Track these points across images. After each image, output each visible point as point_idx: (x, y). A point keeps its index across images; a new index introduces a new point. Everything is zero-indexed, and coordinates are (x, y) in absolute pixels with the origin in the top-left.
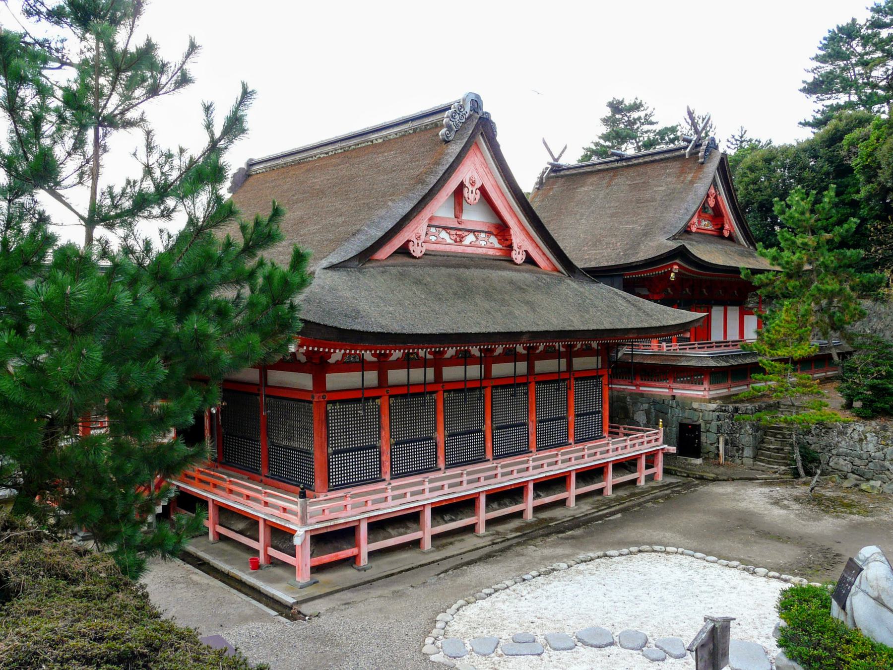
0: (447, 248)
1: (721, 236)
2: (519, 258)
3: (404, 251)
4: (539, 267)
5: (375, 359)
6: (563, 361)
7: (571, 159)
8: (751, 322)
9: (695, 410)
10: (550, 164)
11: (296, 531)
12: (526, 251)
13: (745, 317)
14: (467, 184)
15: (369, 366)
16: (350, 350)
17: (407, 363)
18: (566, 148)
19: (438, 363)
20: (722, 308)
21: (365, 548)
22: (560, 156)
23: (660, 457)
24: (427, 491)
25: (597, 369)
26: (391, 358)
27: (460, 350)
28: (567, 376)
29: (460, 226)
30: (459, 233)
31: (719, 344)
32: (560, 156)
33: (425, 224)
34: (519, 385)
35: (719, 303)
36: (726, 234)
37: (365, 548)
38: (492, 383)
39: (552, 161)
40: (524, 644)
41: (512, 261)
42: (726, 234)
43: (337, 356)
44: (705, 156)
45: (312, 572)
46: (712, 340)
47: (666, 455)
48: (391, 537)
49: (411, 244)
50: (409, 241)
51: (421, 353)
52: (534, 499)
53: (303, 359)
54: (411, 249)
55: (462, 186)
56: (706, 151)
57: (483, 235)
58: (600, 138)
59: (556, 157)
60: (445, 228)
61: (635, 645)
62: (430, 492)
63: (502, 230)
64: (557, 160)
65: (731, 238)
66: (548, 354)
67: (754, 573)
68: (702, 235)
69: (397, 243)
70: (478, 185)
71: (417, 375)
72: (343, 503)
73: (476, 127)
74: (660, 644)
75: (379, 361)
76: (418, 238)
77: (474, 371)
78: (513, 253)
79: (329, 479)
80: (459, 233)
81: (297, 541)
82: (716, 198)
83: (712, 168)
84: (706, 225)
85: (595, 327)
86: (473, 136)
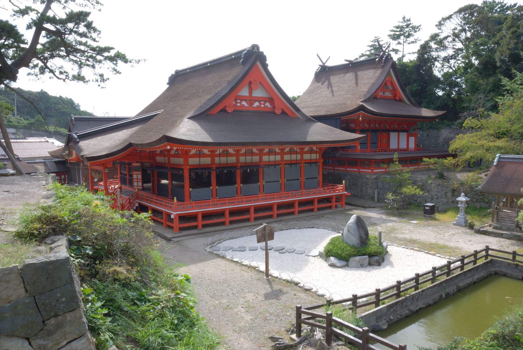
1: (396, 100)
3: (224, 110)
4: (287, 115)
5: (235, 153)
6: (166, 158)
8: (412, 140)
9: (367, 178)
12: (282, 109)
13: (410, 138)
17: (291, 152)
19: (302, 153)
22: (326, 61)
23: (344, 197)
32: (326, 61)
35: (394, 131)
38: (284, 162)
39: (322, 64)
43: (193, 152)
47: (346, 196)
51: (295, 149)
54: (227, 109)
60: (245, 100)
64: (324, 64)
65: (401, 100)
69: (221, 107)
71: (294, 157)
77: (278, 158)
81: (172, 217)
83: (390, 64)
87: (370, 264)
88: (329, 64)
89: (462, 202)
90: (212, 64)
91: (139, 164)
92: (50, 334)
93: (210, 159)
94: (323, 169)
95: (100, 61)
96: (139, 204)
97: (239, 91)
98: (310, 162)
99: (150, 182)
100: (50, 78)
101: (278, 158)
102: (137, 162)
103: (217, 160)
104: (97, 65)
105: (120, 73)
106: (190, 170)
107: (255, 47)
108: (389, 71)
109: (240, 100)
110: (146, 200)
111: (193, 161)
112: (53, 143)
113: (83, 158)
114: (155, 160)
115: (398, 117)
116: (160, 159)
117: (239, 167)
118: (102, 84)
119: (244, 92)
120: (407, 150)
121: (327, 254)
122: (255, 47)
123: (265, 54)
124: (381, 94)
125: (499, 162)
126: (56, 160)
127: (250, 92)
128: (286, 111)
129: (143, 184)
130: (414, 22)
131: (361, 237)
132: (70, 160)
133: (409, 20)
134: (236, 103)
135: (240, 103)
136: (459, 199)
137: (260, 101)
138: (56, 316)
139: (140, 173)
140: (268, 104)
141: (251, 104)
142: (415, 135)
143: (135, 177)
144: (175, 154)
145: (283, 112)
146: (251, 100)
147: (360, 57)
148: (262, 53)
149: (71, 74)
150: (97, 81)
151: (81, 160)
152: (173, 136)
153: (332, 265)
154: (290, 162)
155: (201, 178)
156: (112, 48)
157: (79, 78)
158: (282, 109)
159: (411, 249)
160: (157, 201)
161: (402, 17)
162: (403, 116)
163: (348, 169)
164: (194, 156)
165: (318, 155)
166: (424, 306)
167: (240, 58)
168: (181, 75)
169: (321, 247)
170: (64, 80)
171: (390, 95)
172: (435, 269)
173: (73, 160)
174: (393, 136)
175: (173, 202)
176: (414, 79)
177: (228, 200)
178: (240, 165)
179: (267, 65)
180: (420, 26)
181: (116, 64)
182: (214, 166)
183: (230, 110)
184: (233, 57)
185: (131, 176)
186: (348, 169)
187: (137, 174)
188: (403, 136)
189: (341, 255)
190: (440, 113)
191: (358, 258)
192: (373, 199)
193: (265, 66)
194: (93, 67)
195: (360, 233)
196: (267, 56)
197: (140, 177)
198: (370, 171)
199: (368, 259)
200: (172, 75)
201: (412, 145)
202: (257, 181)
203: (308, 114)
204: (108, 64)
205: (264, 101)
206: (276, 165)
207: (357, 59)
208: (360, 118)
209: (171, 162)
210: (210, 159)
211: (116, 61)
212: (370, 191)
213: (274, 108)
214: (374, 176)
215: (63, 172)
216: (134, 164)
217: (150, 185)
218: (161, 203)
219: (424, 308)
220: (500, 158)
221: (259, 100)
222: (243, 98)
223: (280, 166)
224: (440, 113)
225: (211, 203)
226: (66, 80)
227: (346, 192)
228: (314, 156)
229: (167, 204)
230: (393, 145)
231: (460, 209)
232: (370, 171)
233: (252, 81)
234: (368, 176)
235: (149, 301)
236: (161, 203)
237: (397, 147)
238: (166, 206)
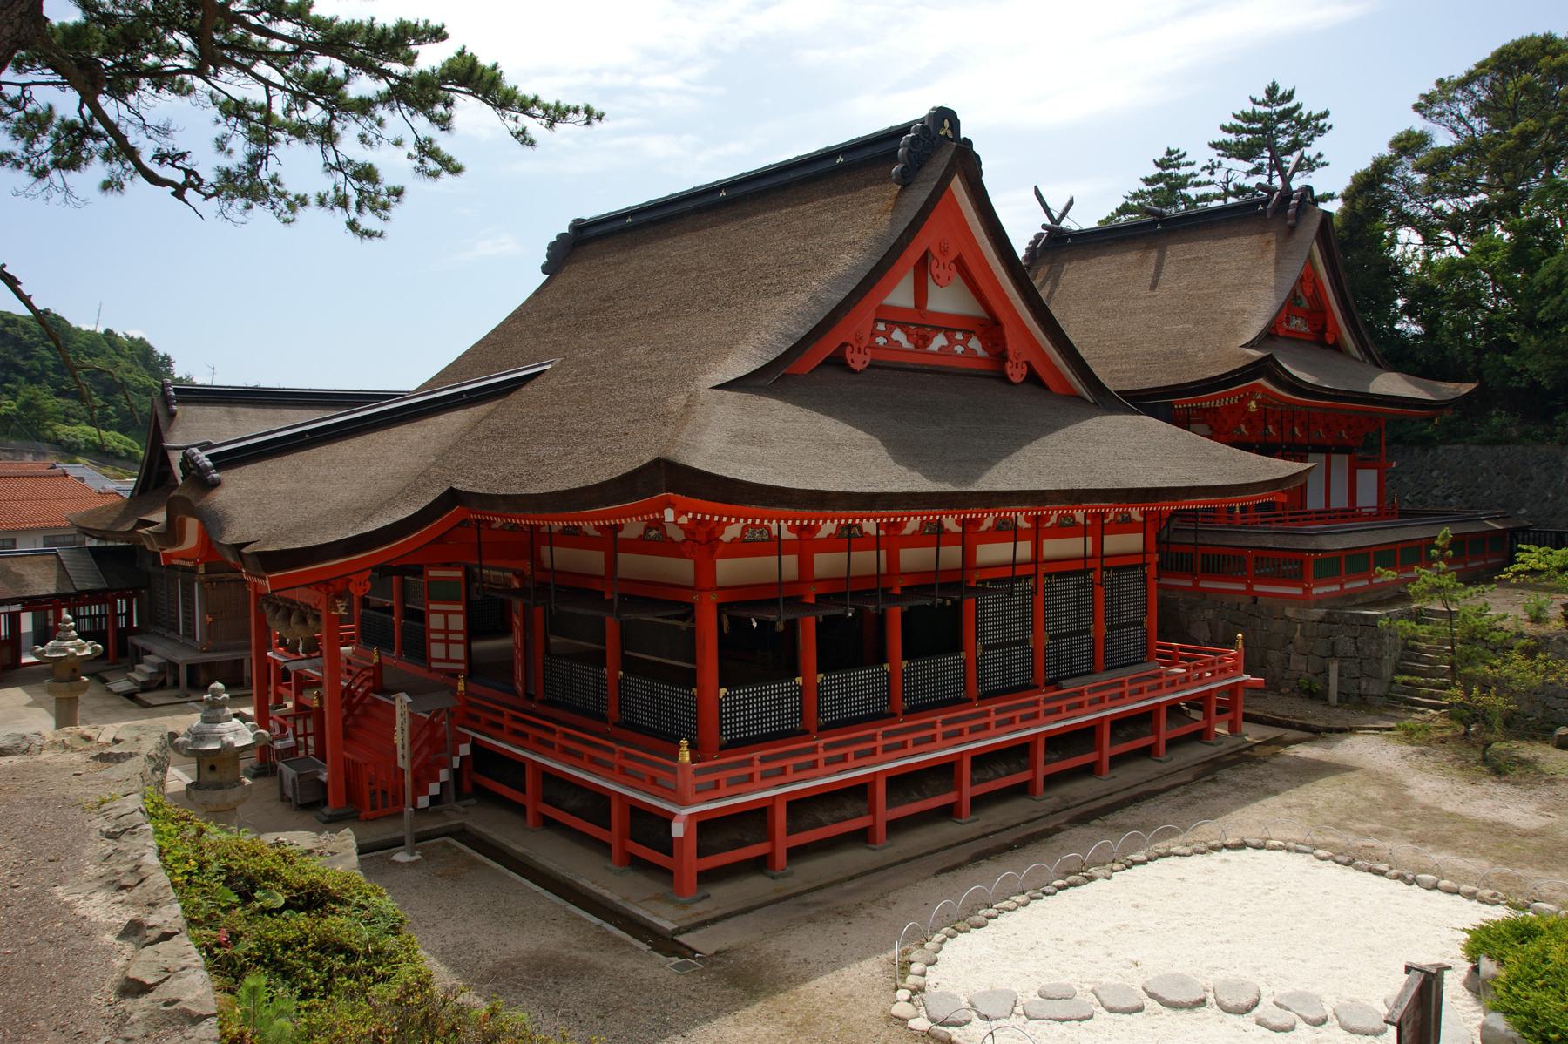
4: (1047, 388)
5: (794, 536)
7: (1083, 219)
8: (1368, 480)
9: (1289, 620)
10: (1044, 227)
11: (674, 815)
12: (1028, 363)
13: (1360, 472)
14: (935, 251)
15: (951, 539)
16: (754, 520)
18: (1071, 203)
20: (1323, 457)
21: (783, 841)
22: (1063, 215)
23: (1241, 695)
24: (880, 750)
25: (1085, 558)
26: (819, 535)
27: (928, 521)
28: (1031, 570)
32: (1063, 215)
36: (1330, 341)
37: (783, 841)
38: (1043, 568)
39: (1048, 223)
40: (1060, 1005)
43: (732, 532)
44: (1297, 216)
45: (699, 882)
47: (1253, 688)
48: (821, 824)
49: (849, 349)
50: (844, 345)
52: (1047, 762)
53: (679, 536)
54: (849, 357)
55: (925, 257)
58: (1425, 106)
60: (903, 326)
61: (1311, 1016)
62: (885, 751)
66: (1065, 529)
68: (1294, 338)
69: (827, 347)
70: (953, 256)
72: (747, 771)
74: (1283, 1002)
75: (800, 539)
76: (859, 339)
78: (1009, 364)
79: (721, 731)
81: (677, 830)
83: (1311, 227)
85: (1146, 485)
88: (1073, 223)
90: (853, 157)
91: (459, 574)
94: (1159, 586)
95: (364, 106)
96: (476, 746)
97: (887, 293)
98: (1123, 564)
100: (107, 186)
101: (1025, 550)
102: (447, 565)
104: (349, 130)
105: (457, 170)
106: (721, 607)
107: (944, 117)
109: (887, 322)
110: (515, 732)
112: (82, 479)
113: (241, 556)
114: (536, 559)
115: (1409, 406)
116: (564, 557)
117: (898, 591)
118: (368, 220)
119: (901, 296)
122: (944, 117)
126: (94, 543)
127: (921, 294)
128: (1043, 372)
129: (468, 644)
130: (1309, 105)
132: (170, 556)
133: (1289, 97)
135: (887, 335)
137: (949, 332)
139: (460, 608)
141: (923, 341)
143: (436, 621)
144: (641, 538)
145: (1033, 378)
146: (921, 323)
147: (1120, 212)
149: (208, 166)
150: (343, 202)
151: (226, 563)
152: (696, 465)
155: (757, 641)
156: (438, 34)
157: (245, 186)
158: (1028, 363)
160: (572, 745)
161: (1268, 83)
163: (1204, 584)
167: (892, 157)
170: (179, 192)
171: (1303, 329)
173: (183, 556)
175: (675, 755)
178: (901, 582)
180: (1326, 115)
181: (444, 123)
182: (814, 589)
183: (858, 361)
185: (420, 617)
186: (1204, 584)
187: (446, 613)
190: (1453, 390)
194: (327, 135)
197: (458, 622)
198: (1299, 591)
200: (561, 237)
202: (955, 646)
203: (1112, 386)
204: (398, 122)
205: (964, 332)
206: (1019, 579)
207: (1109, 219)
208: (1253, 404)
209: (621, 573)
211: (448, 104)
214: (1318, 613)
216: (432, 573)
218: (598, 754)
221: (948, 325)
222: (894, 318)
223: (1031, 582)
224: (1453, 390)
226: (190, 193)
227: (1246, 677)
228: (1132, 542)
229: (631, 765)
232: (1299, 591)
234: (1290, 612)
236: (598, 754)
237: (1323, 507)
238: (623, 771)
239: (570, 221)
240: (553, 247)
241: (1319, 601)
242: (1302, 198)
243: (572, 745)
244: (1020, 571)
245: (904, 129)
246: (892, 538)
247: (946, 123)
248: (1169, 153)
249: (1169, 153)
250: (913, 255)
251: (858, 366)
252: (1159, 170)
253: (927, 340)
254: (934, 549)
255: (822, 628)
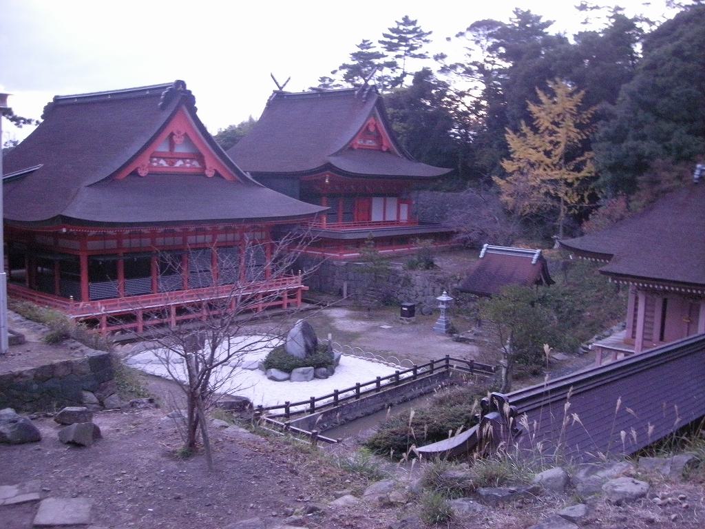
0: (165, 170)
2: (210, 174)
8: (404, 209)
9: (334, 265)
10: (275, 92)
18: (289, 79)
22: (285, 85)
23: (299, 292)
29: (172, 156)
30: (172, 158)
31: (378, 223)
32: (285, 85)
33: (148, 157)
34: (200, 249)
35: (378, 195)
36: (385, 149)
41: (205, 176)
42: (385, 149)
43: (93, 233)
46: (373, 220)
47: (303, 291)
55: (172, 134)
56: (368, 94)
57: (188, 161)
59: (281, 85)
60: (164, 158)
63: (199, 157)
64: (281, 88)
65: (389, 151)
67: (388, 365)
69: (131, 169)
70: (183, 133)
73: (177, 99)
80: (172, 158)
82: (375, 126)
83: (373, 102)
84: (370, 143)
86: (178, 108)
87: (316, 377)
88: (291, 88)
89: (443, 302)
92: (102, 390)
93: (115, 241)
99: (22, 267)
103: (126, 243)
107: (180, 83)
108: (373, 109)
111: (93, 245)
119: (163, 148)
120: (397, 222)
121: (267, 365)
122: (180, 83)
123: (193, 93)
124: (360, 142)
125: (486, 253)
131: (307, 346)
134: (151, 162)
136: (440, 298)
137: (183, 159)
138: (104, 382)
140: (196, 163)
142: (408, 202)
148: (190, 92)
153: (273, 378)
154: (224, 244)
159: (369, 360)
162: (388, 177)
164: (94, 238)
165: (264, 233)
166: (362, 415)
168: (62, 106)
169: (262, 355)
171: (374, 144)
172: (379, 379)
174: (377, 204)
176: (416, 116)
177: (142, 298)
179: (196, 109)
184: (148, 93)
188: (392, 203)
189: (280, 365)
190: (446, 170)
191: (301, 369)
192: (340, 293)
193: (193, 110)
195: (305, 341)
196: (196, 97)
199: (313, 370)
200: (49, 104)
201: (404, 216)
210: (115, 241)
212: (337, 283)
213: (205, 168)
215: (630, 499)
217: (23, 271)
219: (361, 417)
220: (488, 249)
224: (446, 170)
225: (119, 302)
230: (376, 216)
231: (442, 310)
233: (175, 132)
234: (335, 263)
235: (321, 285)
239: (53, 97)
240: (46, 108)
241: (345, 259)
242: (370, 90)
243: (41, 300)
244: (229, 244)
245: (163, 88)
246: (153, 235)
247: (181, 86)
248: (364, 41)
249: (364, 41)
250: (166, 134)
251: (143, 175)
252: (360, 50)
253: (173, 163)
254: (225, 235)
255: (125, 263)
